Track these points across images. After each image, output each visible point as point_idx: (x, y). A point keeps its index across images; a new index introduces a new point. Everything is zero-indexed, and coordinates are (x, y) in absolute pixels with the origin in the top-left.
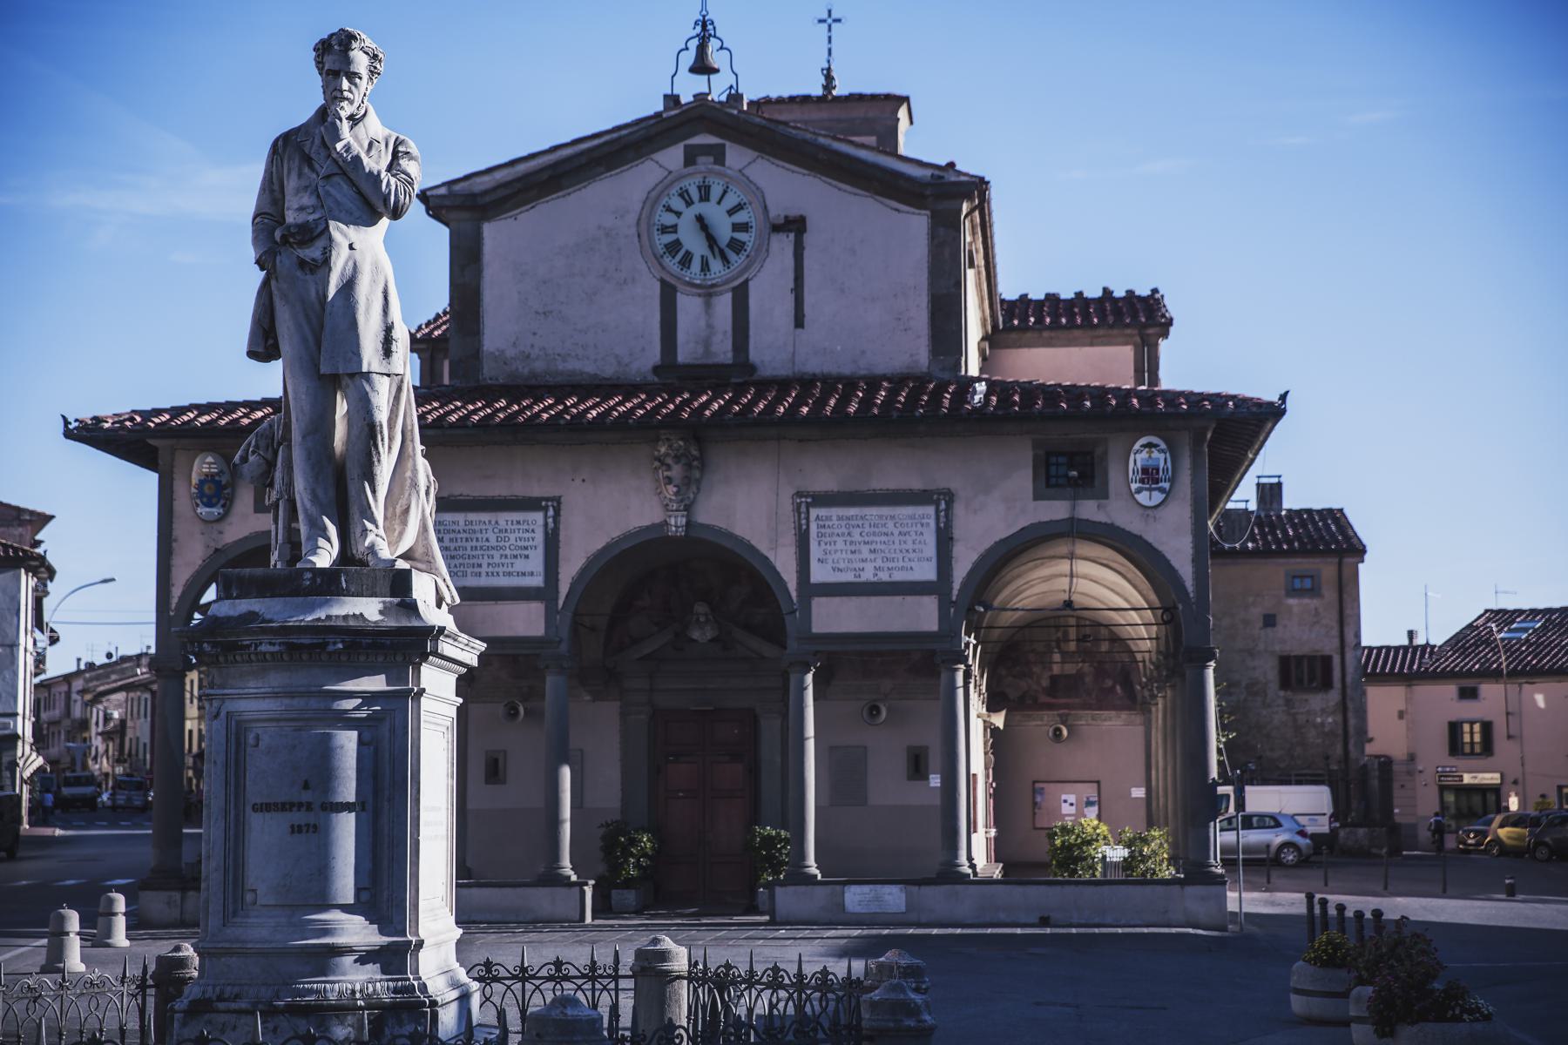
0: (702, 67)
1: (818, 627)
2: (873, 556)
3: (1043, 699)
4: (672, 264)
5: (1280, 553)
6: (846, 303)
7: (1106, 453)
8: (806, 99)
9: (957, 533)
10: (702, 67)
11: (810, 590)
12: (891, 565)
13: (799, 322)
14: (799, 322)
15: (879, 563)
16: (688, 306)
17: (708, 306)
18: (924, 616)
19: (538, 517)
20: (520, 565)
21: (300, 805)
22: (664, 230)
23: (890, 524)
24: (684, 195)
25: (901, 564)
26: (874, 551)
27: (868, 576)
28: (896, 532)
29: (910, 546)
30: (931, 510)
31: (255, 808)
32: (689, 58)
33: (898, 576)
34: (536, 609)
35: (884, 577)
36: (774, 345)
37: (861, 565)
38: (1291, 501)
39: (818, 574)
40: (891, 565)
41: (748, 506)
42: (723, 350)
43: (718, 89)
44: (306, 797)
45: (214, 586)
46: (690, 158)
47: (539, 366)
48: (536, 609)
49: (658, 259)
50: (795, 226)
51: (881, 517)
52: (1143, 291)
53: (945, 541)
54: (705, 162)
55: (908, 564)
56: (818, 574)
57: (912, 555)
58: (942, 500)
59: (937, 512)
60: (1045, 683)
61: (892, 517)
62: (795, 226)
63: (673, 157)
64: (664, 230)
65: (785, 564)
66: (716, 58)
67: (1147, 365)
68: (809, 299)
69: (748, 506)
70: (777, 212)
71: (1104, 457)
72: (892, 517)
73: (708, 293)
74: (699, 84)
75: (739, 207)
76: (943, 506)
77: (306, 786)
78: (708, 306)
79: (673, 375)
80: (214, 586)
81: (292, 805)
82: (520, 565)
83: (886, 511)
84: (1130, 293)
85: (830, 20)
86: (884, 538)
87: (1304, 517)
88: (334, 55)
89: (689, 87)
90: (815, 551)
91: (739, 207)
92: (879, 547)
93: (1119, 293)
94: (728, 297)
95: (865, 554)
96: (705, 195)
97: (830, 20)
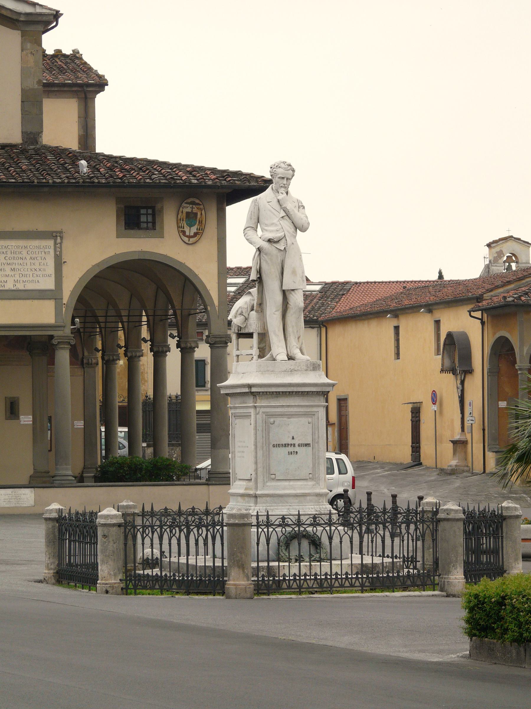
2: (12, 273)
7: (162, 208)
9: (65, 258)
12: (25, 279)
13: (398, 355)
14: (398, 355)
15: (17, 278)
18: (42, 314)
21: (291, 444)
23: (24, 252)
25: (31, 278)
26: (13, 270)
27: (9, 286)
28: (28, 257)
29: (37, 267)
30: (51, 243)
31: (274, 446)
33: (30, 286)
34: (49, 306)
35: (20, 286)
37: (5, 279)
38: (446, 278)
40: (25, 279)
44: (293, 442)
48: (49, 306)
51: (18, 247)
53: (59, 263)
55: (36, 279)
57: (39, 273)
58: (55, 236)
59: (55, 244)
61: (26, 247)
71: (161, 210)
72: (26, 247)
76: (59, 240)
77: (293, 438)
81: (288, 444)
83: (21, 243)
86: (20, 261)
92: (17, 267)
95: (8, 272)
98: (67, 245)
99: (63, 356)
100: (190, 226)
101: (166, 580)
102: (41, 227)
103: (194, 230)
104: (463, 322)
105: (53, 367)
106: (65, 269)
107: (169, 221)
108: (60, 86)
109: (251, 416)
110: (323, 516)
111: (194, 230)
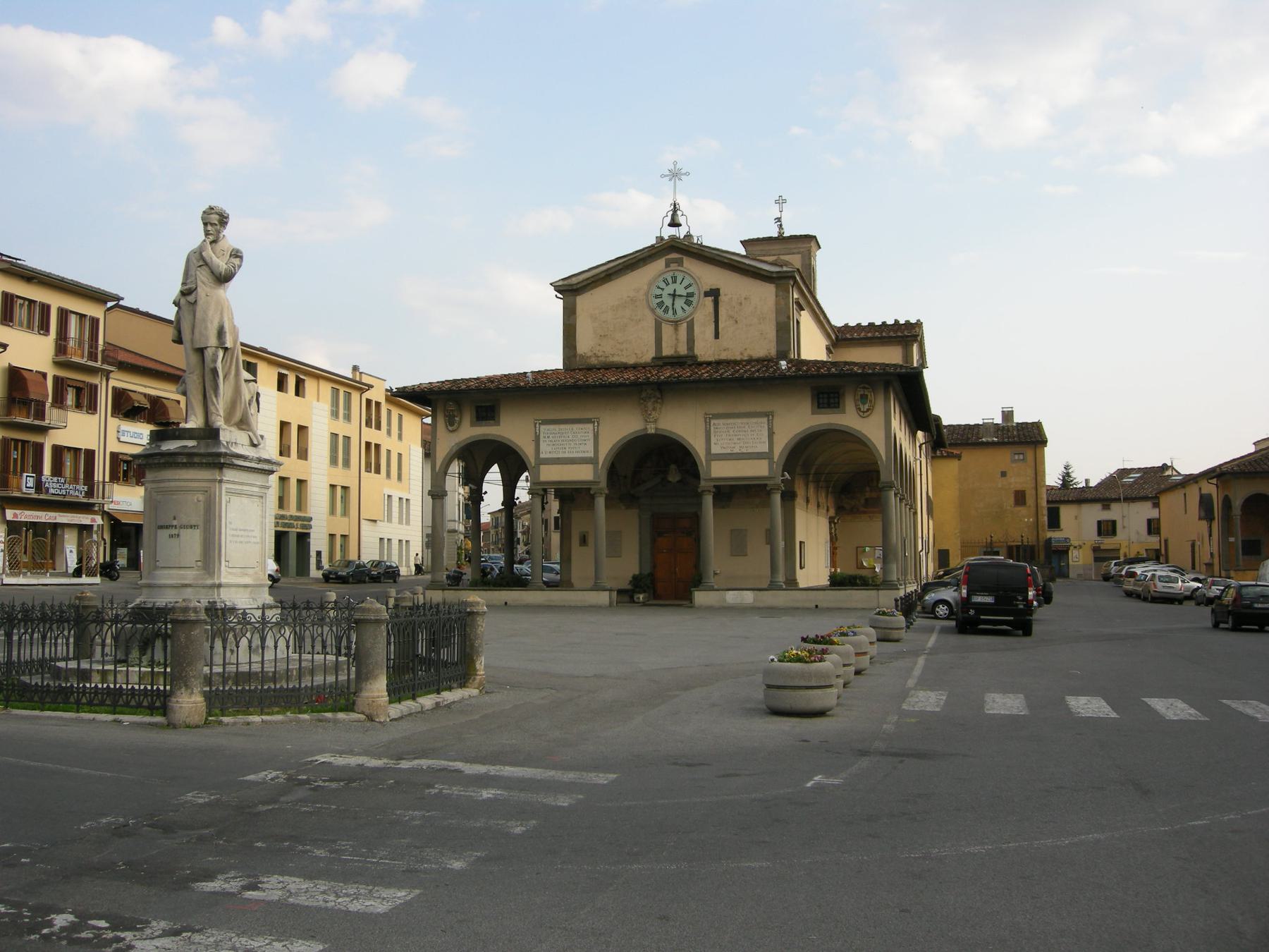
0: (674, 224)
1: (140, 491)
3: (862, 509)
4: (660, 312)
5: (1009, 443)
6: (743, 330)
8: (770, 239)
9: (775, 430)
10: (674, 224)
11: (711, 457)
13: (717, 336)
14: (717, 336)
16: (667, 330)
17: (676, 329)
18: (759, 469)
19: (590, 426)
20: (582, 448)
22: (657, 297)
24: (666, 281)
27: (736, 450)
30: (765, 420)
32: (668, 220)
34: (590, 467)
36: (706, 349)
38: (1018, 419)
39: (715, 449)
41: (682, 422)
42: (683, 350)
43: (681, 232)
45: (495, 468)
46: (667, 265)
47: (603, 359)
49: (653, 311)
50: (714, 294)
52: (913, 321)
53: (771, 434)
54: (673, 266)
56: (715, 449)
58: (768, 415)
60: (863, 501)
62: (714, 294)
63: (660, 264)
64: (657, 297)
65: (697, 445)
66: (681, 220)
67: (907, 356)
68: (721, 325)
69: (682, 422)
70: (707, 288)
73: (676, 324)
74: (673, 231)
75: (690, 285)
78: (676, 329)
79: (661, 362)
80: (495, 468)
82: (582, 448)
83: (745, 420)
84: (884, 323)
85: (781, 201)
87: (1023, 426)
88: (215, 221)
89: (668, 232)
90: (713, 440)
91: (690, 285)
93: (902, 322)
94: (685, 325)
96: (674, 282)
97: (781, 201)
98: (777, 423)
99: (600, 502)
100: (864, 404)
101: (48, 691)
102: (759, 409)
103: (866, 407)
104: (1210, 488)
105: (279, 529)
106: (775, 437)
107: (849, 404)
108: (91, 347)
109: (1048, 502)
110: (254, 612)
111: (866, 407)
